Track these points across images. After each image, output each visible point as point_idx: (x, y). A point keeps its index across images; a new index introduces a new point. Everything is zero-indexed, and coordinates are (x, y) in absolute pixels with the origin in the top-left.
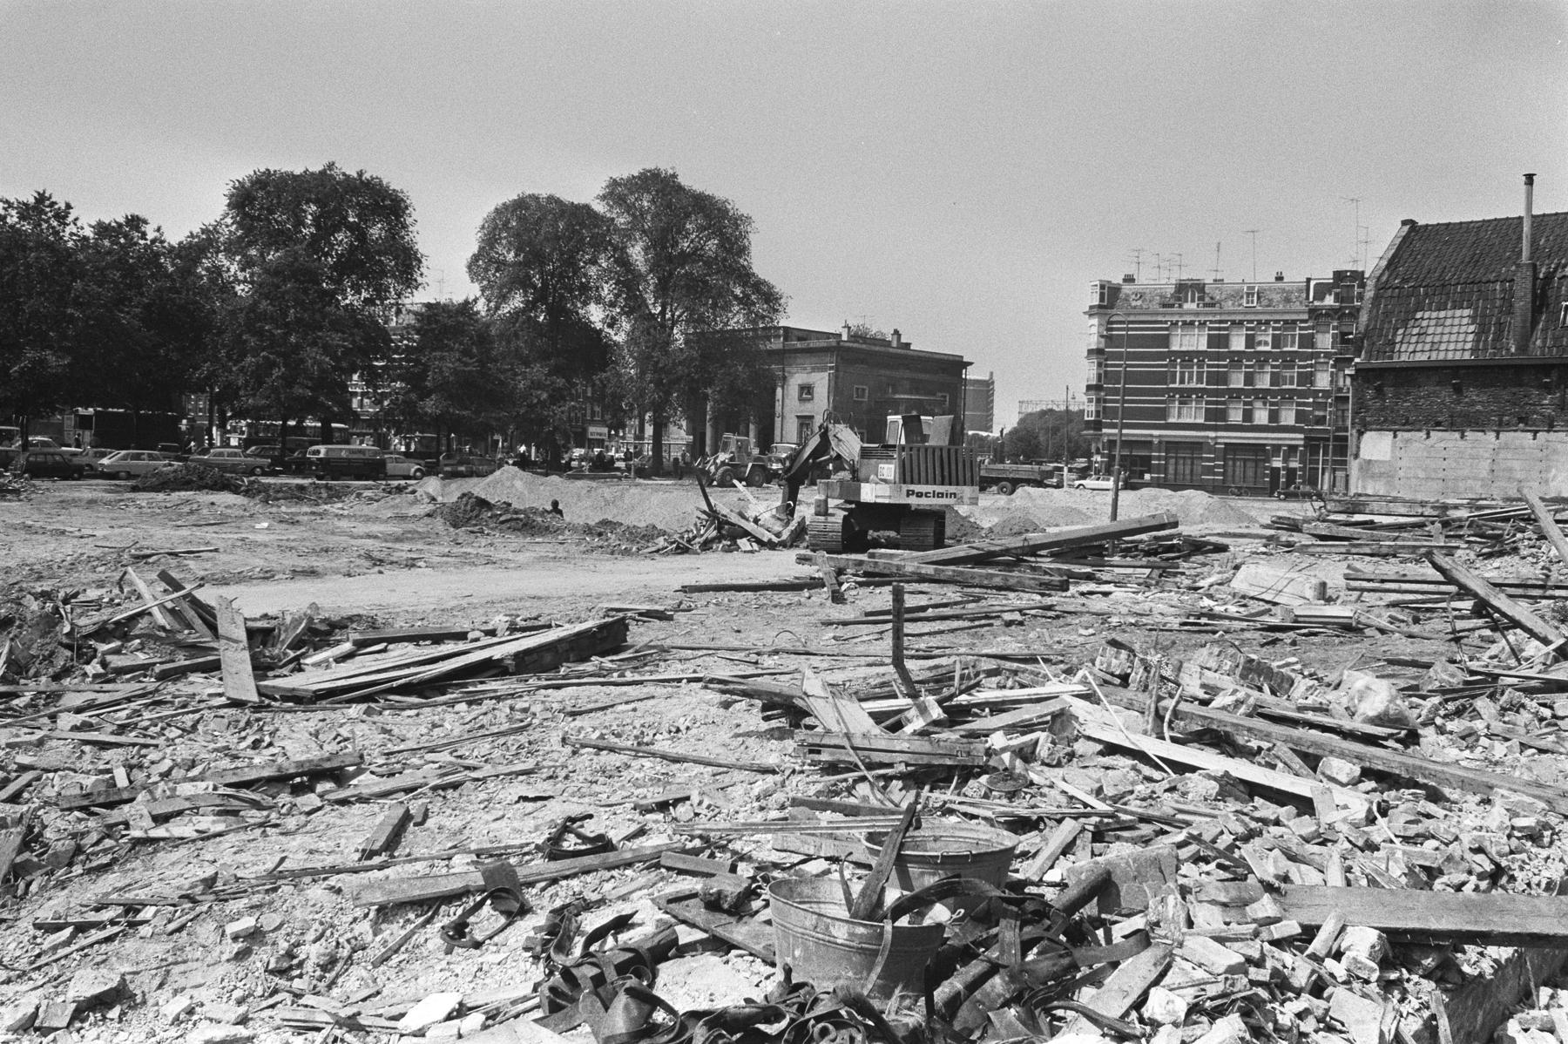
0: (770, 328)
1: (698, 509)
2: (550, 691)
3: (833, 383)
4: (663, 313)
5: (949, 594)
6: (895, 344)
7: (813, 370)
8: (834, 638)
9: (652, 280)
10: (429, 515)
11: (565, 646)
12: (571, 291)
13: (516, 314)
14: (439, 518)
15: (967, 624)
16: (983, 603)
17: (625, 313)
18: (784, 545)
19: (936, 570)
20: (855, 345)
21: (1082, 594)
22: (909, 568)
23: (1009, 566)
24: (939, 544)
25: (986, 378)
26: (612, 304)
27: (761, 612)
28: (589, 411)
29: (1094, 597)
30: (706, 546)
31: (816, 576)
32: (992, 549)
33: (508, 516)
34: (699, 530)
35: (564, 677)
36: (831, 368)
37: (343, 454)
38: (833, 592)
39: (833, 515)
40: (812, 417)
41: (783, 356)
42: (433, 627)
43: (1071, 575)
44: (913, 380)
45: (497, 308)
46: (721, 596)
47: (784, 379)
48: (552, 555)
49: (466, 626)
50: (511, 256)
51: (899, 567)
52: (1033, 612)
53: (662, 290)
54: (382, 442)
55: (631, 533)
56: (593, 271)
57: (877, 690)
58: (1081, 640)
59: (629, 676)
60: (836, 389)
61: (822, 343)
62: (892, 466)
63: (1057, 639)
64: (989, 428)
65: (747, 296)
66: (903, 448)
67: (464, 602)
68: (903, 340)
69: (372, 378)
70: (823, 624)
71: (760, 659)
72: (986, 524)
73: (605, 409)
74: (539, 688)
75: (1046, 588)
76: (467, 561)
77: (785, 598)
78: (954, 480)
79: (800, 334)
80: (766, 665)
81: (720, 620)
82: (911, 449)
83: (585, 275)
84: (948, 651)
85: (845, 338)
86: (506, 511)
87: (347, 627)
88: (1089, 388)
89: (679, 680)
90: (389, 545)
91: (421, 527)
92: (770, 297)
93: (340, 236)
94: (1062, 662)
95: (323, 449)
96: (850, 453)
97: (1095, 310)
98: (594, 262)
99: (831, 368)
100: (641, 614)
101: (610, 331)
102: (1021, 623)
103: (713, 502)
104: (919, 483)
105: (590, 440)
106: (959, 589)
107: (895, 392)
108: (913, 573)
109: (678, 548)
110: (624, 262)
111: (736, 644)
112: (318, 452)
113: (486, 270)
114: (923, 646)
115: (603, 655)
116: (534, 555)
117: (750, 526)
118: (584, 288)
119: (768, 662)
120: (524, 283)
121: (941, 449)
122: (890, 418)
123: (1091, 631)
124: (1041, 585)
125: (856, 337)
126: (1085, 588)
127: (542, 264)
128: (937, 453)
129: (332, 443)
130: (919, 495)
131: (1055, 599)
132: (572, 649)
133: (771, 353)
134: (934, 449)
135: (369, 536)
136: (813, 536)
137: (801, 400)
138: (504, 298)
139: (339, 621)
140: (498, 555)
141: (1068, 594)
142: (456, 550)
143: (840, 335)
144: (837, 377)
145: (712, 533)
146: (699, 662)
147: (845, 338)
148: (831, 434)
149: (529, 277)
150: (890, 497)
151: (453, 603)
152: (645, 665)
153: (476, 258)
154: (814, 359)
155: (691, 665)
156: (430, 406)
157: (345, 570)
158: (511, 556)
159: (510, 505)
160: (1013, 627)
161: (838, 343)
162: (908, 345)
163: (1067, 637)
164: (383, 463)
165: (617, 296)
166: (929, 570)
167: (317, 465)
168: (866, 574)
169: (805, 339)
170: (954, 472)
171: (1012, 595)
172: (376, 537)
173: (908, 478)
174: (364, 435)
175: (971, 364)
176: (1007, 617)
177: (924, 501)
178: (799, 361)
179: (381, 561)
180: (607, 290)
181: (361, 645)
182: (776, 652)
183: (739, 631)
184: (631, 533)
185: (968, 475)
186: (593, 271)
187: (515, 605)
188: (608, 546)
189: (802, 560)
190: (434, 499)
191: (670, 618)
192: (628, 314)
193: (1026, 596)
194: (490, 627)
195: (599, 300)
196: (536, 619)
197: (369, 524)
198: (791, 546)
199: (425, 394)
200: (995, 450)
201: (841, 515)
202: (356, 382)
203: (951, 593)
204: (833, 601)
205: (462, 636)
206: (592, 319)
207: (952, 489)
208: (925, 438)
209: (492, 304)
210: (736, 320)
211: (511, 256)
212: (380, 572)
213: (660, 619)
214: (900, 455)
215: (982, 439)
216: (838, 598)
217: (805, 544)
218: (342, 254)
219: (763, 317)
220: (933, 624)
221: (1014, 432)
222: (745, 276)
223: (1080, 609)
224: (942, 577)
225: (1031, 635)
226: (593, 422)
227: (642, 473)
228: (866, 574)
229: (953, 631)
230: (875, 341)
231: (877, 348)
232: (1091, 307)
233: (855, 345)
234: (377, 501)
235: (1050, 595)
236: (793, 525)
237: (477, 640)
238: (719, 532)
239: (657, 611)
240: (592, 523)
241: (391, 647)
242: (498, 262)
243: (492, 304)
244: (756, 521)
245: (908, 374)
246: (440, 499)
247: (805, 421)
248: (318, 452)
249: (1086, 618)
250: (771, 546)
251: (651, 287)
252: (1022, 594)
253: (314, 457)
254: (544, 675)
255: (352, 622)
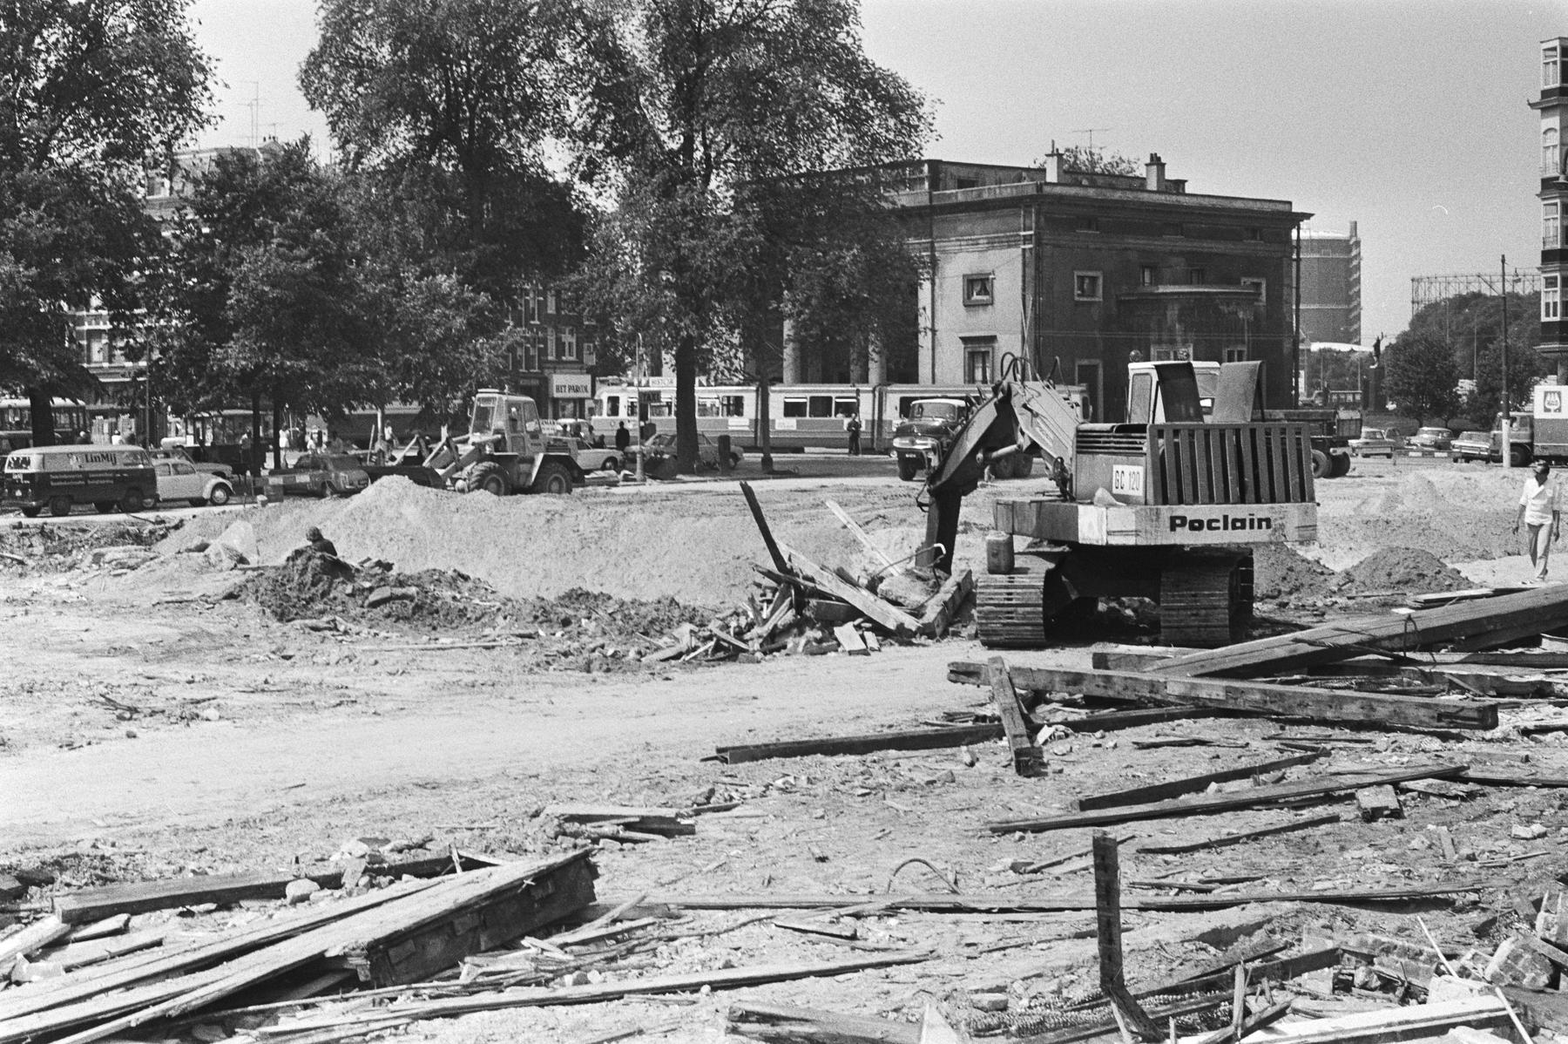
0: (903, 165)
1: (756, 567)
2: (438, 1022)
3: (1031, 271)
4: (688, 148)
5: (1254, 744)
6: (1152, 185)
7: (992, 244)
8: (1015, 868)
9: (666, 88)
10: (231, 596)
11: (469, 920)
12: (506, 113)
13: (396, 167)
14: (251, 602)
15: (1283, 817)
16: (1321, 765)
17: (614, 152)
18: (928, 632)
19: (1228, 690)
20: (1072, 191)
21: (1526, 732)
22: (1175, 688)
23: (1376, 675)
24: (1243, 625)
25: (1343, 234)
26: (588, 136)
27: (871, 806)
28: (551, 346)
29: (1549, 737)
30: (774, 642)
31: (987, 711)
32: (1343, 640)
33: (385, 592)
34: (758, 611)
35: (471, 989)
36: (1026, 239)
37: (74, 465)
38: (1019, 753)
39: (1024, 571)
40: (993, 339)
41: (925, 219)
42: (223, 874)
43: (1503, 689)
44: (1191, 256)
45: (359, 156)
46: (793, 765)
47: (934, 264)
48: (469, 678)
49: (284, 872)
50: (384, 53)
51: (1153, 686)
52: (1420, 785)
53: (686, 107)
54: (149, 433)
55: (627, 618)
56: (546, 72)
57: (1085, 1015)
58: (1517, 849)
59: (598, 982)
60: (1039, 278)
61: (1007, 191)
62: (1140, 469)
63: (1465, 851)
64: (1352, 336)
65: (854, 104)
66: (1160, 432)
67: (287, 801)
68: (1170, 175)
69: (121, 304)
70: (994, 830)
71: (861, 927)
72: (1339, 561)
73: (585, 336)
74: (416, 1017)
75: (1450, 725)
76: (299, 698)
77: (917, 765)
78: (1265, 490)
79: (963, 173)
80: (870, 944)
81: (788, 828)
82: (1176, 433)
83: (533, 81)
84: (1243, 890)
85: (1052, 176)
86: (383, 581)
87: (51, 881)
88: (1548, 256)
89: (694, 988)
90: (153, 669)
91: (213, 622)
92: (897, 102)
93: (52, 35)
94: (1475, 905)
95: (34, 454)
96: (1056, 440)
97: (1554, 100)
98: (548, 53)
99: (1026, 239)
100: (629, 826)
101: (585, 187)
102: (1396, 814)
103: (784, 551)
104: (1195, 501)
105: (556, 401)
106: (1273, 729)
107: (1157, 281)
108: (1182, 697)
109: (717, 648)
110: (609, 52)
111: (816, 893)
112: (27, 462)
113: (338, 82)
114: (1193, 878)
115: (545, 932)
116: (432, 678)
117: (860, 599)
118: (530, 106)
119: (876, 932)
120: (415, 104)
121: (1237, 431)
122: (1134, 367)
123: (1537, 828)
124: (1440, 717)
125: (1072, 171)
126: (1532, 715)
127: (445, 64)
128: (1230, 440)
129: (52, 442)
130: (1196, 526)
131: (1467, 750)
132: (484, 926)
133: (905, 214)
134: (1222, 431)
135: (113, 651)
136: (986, 615)
137: (969, 305)
138: (376, 136)
139: (39, 870)
140: (360, 684)
141: (1497, 733)
142: (285, 675)
143: (1042, 171)
144: (1038, 258)
145: (785, 616)
146: (738, 937)
147: (1052, 176)
148: (1016, 403)
149: (421, 92)
150: (1137, 533)
151: (267, 804)
152: (630, 951)
153: (315, 61)
154: (993, 223)
155: (719, 949)
156: (234, 355)
157: (62, 734)
158: (387, 684)
159: (389, 567)
160: (1380, 824)
161: (1039, 188)
162: (1180, 184)
163: (1488, 844)
164: (149, 477)
165: (597, 118)
166: (1214, 690)
167: (24, 488)
168: (1091, 702)
169: (972, 184)
170: (1264, 478)
171: (1381, 740)
172: (128, 651)
173: (1172, 493)
174: (116, 414)
175: (1308, 216)
176: (1368, 799)
177: (1205, 538)
178: (962, 228)
179: (133, 710)
180: (575, 110)
181: (78, 919)
182: (892, 911)
183: (823, 859)
184: (627, 618)
185: (1294, 481)
186: (546, 72)
187: (384, 806)
188: (580, 651)
189: (962, 673)
190: (242, 560)
191: (690, 831)
192: (619, 153)
193: (1411, 741)
194: (329, 870)
195: (561, 129)
196: (421, 846)
197: (117, 622)
198: (944, 634)
199: (220, 332)
200: (1365, 384)
201: (1039, 569)
202: (95, 315)
203: (1257, 741)
204: (1019, 771)
205: (274, 891)
206: (549, 166)
207: (1262, 510)
208: (1200, 412)
209: (352, 147)
210: (837, 152)
211: (384, 53)
212: (131, 736)
213: (668, 834)
214: (1154, 446)
215: (1339, 358)
216: (1029, 764)
217: (972, 629)
218: (58, 71)
219: (888, 145)
220: (1216, 819)
221: (1405, 342)
222: (850, 69)
223: (1520, 773)
224: (1242, 705)
225: (1415, 844)
226: (559, 365)
227: (655, 469)
228: (1091, 702)
229: (1256, 837)
230: (1116, 179)
231: (1118, 195)
232: (1545, 94)
233: (1072, 191)
234: (133, 568)
235: (1459, 738)
236: (949, 587)
237: (304, 898)
238: (799, 612)
239: (662, 819)
240: (551, 597)
241: (136, 921)
242: (358, 64)
243: (352, 147)
244: (872, 586)
245: (1182, 244)
246: (253, 560)
247: (978, 349)
248: (27, 462)
249: (1532, 795)
250: (902, 636)
251: (665, 98)
252: (1402, 738)
253: (18, 473)
254: (426, 988)
255: (63, 869)
